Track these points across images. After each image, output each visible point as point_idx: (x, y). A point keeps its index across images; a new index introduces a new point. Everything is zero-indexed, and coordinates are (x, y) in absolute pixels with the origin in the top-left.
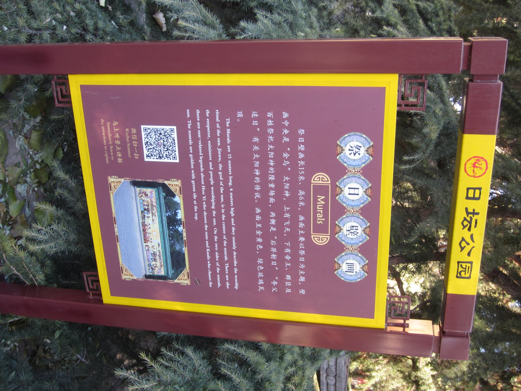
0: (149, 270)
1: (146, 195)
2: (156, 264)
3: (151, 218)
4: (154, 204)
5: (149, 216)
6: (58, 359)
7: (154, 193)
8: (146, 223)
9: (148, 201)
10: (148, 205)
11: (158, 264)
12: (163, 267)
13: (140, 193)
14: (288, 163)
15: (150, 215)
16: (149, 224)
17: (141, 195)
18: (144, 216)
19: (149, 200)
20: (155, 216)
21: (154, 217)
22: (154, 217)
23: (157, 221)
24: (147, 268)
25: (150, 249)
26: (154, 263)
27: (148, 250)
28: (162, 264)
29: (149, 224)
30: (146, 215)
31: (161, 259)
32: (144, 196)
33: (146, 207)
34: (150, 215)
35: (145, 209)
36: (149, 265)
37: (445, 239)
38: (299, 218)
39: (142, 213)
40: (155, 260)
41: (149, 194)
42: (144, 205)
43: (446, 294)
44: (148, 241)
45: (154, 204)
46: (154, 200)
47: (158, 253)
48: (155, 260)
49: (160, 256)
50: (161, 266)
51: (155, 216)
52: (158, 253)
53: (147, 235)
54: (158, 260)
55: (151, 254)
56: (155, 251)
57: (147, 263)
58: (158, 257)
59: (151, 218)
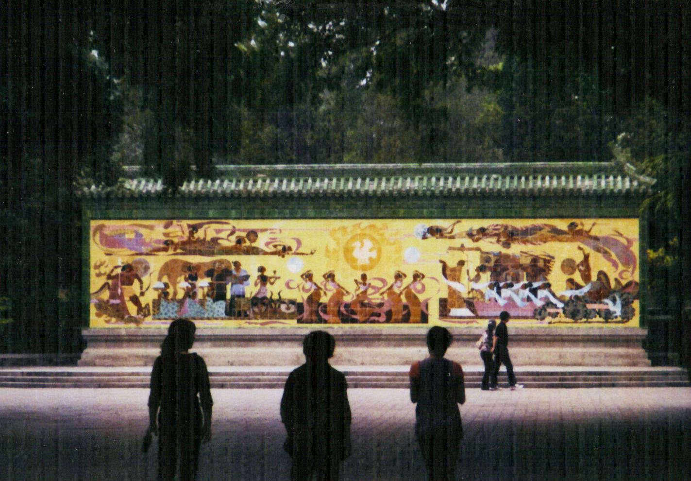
0: (608, 316)
1: (130, 274)
2: (569, 266)
3: (272, 264)
5: (254, 275)
6: (516, 57)
7: (112, 226)
8: (301, 297)
9: (167, 270)
11: (565, 251)
12: (587, 224)
13: (120, 312)
15: (250, 265)
16: (308, 276)
17: (132, 309)
18: (256, 301)
19: (156, 262)
20: (253, 234)
21: (260, 243)
22: (260, 243)
23: (286, 230)
24: (596, 326)
25: (462, 288)
26: (557, 278)
27: (470, 304)
28: (562, 225)
29: (308, 276)
30: (250, 289)
31: (526, 232)
32: (135, 288)
33: (204, 283)
34: (250, 265)
35: (218, 293)
36: (576, 309)
38: (366, 74)
40: (538, 269)
42: (191, 293)
43: (208, 209)
44: (412, 297)
45: (179, 230)
46: (156, 231)
47: (491, 246)
48: (538, 269)
49: (511, 236)
50: (576, 233)
51: (253, 234)
53: (375, 298)
54: (539, 250)
55: (495, 286)
56: (474, 261)
57: (564, 326)
58: (516, 249)
59: (272, 264)
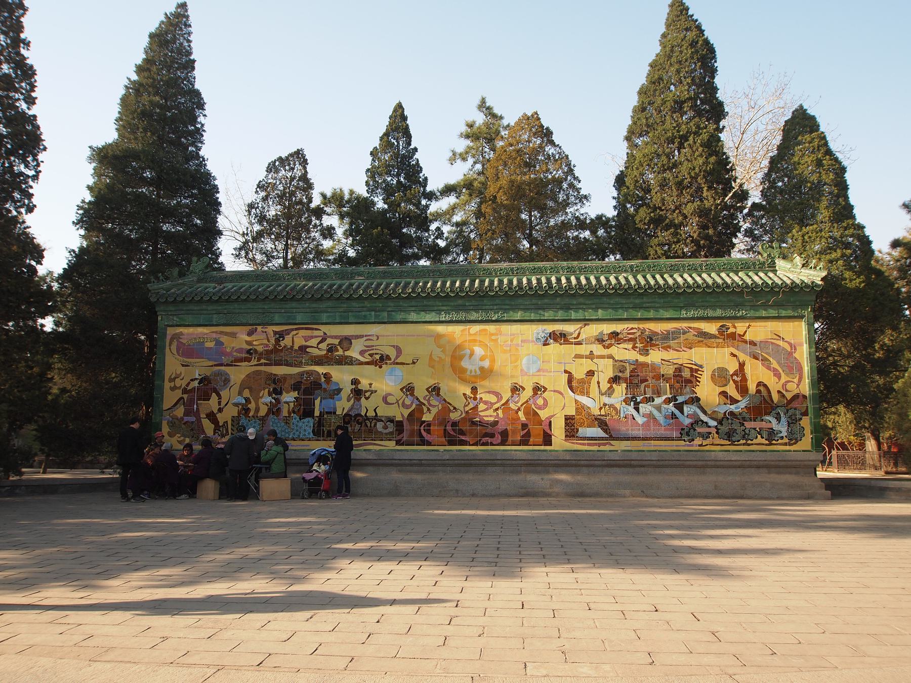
0: (771, 435)
1: (208, 387)
2: (720, 376)
4: (262, 339)
5: (347, 388)
7: (189, 333)
8: (399, 413)
9: (248, 384)
10: (277, 386)
11: (713, 358)
14: (17, 442)
15: (342, 376)
19: (238, 374)
20: (346, 341)
21: (354, 353)
22: (354, 353)
23: (385, 335)
25: (592, 403)
28: (711, 328)
29: (409, 390)
30: (343, 405)
31: (675, 334)
33: (289, 397)
34: (342, 376)
37: (33, 161)
39: (402, 444)
41: (200, 369)
42: (275, 410)
45: (262, 339)
46: (240, 338)
47: (625, 353)
49: (649, 342)
51: (346, 341)
52: (625, 353)
53: (488, 415)
56: (606, 370)
58: (655, 356)
59: (368, 377)
